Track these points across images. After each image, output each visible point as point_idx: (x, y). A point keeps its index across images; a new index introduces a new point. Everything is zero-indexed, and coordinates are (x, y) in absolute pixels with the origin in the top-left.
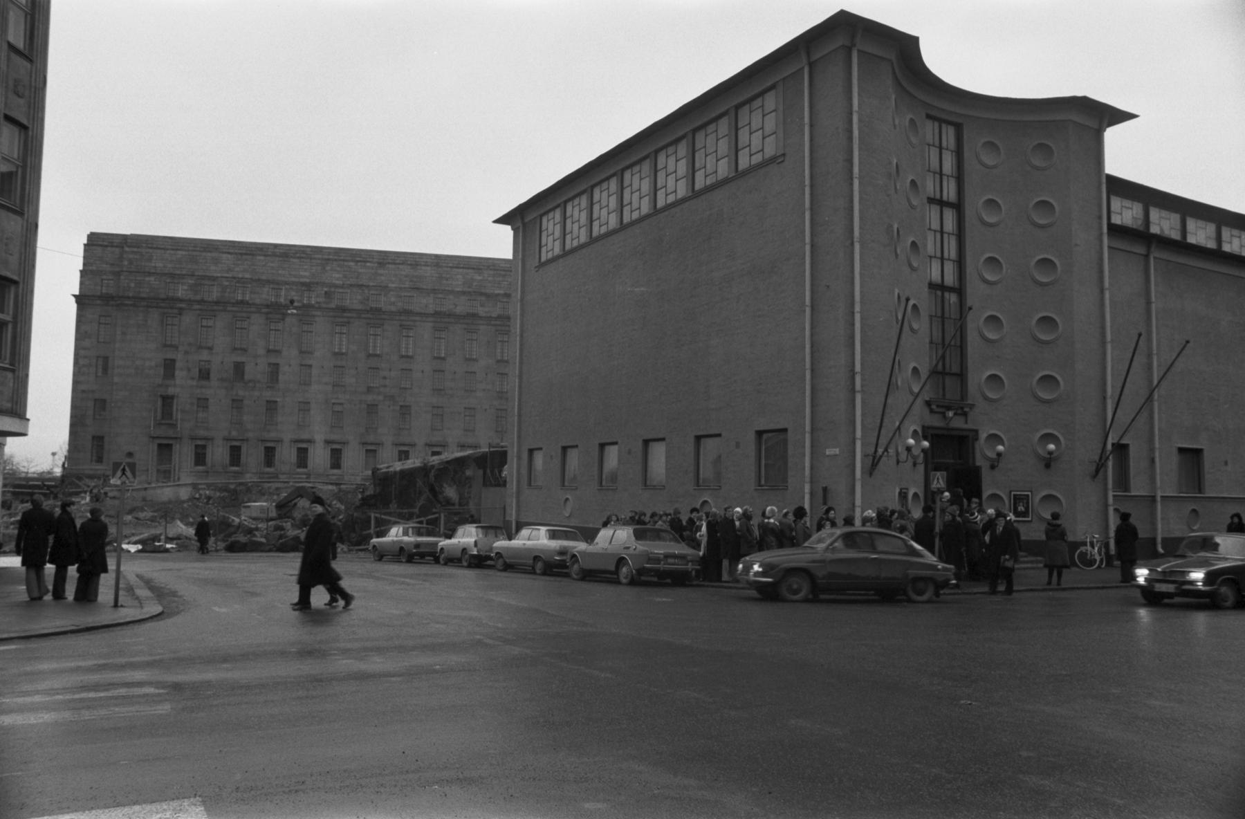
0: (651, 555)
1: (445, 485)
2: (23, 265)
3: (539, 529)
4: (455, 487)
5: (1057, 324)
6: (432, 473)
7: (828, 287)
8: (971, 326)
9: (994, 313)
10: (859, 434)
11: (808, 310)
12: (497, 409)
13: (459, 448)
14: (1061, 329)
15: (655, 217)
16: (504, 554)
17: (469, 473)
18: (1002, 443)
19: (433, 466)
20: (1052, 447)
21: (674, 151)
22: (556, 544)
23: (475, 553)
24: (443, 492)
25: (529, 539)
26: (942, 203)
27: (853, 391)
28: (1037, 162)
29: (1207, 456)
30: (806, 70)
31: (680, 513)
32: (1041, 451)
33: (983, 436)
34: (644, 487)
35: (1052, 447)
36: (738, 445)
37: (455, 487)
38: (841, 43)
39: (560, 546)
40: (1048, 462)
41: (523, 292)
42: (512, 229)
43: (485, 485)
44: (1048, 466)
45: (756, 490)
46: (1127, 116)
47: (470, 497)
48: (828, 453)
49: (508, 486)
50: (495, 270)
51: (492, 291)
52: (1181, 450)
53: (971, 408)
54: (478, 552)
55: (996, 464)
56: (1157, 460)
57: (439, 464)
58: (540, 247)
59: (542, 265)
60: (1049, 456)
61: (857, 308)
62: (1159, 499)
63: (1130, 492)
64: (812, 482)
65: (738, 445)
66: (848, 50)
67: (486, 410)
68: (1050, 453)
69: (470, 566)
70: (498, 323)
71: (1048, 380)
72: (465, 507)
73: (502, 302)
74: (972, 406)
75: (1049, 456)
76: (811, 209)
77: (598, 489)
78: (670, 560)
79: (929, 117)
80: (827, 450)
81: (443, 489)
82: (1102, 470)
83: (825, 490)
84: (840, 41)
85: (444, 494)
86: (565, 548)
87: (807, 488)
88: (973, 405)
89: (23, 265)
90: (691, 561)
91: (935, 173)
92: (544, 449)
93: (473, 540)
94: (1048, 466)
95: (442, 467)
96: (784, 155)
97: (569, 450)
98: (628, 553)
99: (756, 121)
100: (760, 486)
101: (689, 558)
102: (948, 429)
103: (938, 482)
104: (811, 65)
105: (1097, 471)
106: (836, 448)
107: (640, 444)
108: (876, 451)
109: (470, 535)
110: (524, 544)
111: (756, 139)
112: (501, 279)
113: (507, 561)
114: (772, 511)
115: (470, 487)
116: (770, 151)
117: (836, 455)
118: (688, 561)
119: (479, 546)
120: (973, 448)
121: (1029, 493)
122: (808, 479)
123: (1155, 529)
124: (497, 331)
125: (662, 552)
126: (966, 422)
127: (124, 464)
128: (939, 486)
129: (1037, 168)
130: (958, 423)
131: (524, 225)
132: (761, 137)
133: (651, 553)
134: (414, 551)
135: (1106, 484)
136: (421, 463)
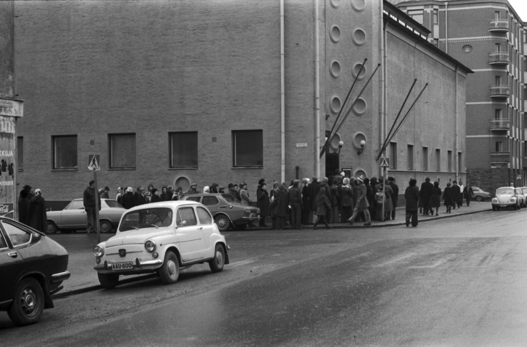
0: (246, 211)
2: (383, 52)
5: (365, 38)
7: (297, 44)
11: (282, 57)
16: (56, 222)
18: (364, 139)
20: (363, 142)
27: (315, 109)
34: (109, 169)
35: (363, 142)
36: (214, 140)
45: (233, 169)
48: (298, 145)
52: (234, 132)
55: (361, 152)
60: (361, 147)
63: (396, 169)
64: (286, 164)
65: (214, 140)
75: (361, 147)
77: (52, 171)
80: (297, 144)
83: (297, 168)
87: (283, 167)
89: (383, 52)
98: (226, 210)
103: (384, 163)
106: (304, 142)
114: (347, 180)
118: (257, 214)
121: (350, 170)
122: (283, 162)
127: (94, 156)
128: (385, 165)
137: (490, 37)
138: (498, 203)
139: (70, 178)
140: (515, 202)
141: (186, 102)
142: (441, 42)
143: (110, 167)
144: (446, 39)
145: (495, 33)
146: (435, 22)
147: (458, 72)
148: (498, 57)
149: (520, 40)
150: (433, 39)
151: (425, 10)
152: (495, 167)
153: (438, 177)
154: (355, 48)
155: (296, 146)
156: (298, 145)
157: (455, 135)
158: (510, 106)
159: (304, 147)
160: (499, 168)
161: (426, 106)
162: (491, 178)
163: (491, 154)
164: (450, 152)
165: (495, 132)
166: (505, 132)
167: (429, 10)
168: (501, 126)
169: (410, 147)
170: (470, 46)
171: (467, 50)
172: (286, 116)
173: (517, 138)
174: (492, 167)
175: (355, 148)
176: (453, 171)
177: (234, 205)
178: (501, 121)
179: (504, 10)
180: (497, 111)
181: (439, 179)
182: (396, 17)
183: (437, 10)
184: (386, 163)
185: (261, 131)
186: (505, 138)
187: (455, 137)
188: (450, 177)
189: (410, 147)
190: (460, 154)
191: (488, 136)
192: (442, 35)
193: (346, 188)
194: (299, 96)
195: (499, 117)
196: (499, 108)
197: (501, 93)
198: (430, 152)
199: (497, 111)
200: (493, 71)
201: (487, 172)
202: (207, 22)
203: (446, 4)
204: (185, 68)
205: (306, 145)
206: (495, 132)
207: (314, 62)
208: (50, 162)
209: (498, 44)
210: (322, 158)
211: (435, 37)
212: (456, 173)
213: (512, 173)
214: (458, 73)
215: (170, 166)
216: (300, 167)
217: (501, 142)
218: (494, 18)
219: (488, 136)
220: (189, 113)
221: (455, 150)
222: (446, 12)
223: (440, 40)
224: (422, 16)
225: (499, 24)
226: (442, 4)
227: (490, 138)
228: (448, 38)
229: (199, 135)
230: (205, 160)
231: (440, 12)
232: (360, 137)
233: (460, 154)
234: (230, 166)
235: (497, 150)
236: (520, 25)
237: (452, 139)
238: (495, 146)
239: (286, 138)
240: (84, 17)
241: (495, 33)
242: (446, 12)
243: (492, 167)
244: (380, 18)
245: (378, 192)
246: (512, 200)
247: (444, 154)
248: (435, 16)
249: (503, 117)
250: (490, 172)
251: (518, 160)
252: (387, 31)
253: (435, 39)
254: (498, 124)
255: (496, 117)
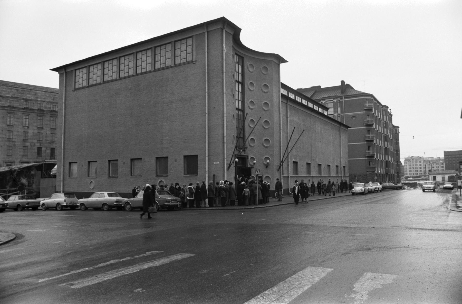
1: (21, 178)
3: (104, 193)
4: (26, 179)
6: (16, 173)
7: (214, 108)
8: (246, 122)
9: (252, 119)
10: (226, 157)
11: (207, 115)
12: (8, 146)
13: (21, 163)
14: (270, 125)
15: (137, 77)
16: (85, 204)
17: (33, 173)
19: (15, 170)
20: (268, 161)
21: (146, 53)
22: (114, 199)
23: (65, 204)
24: (21, 181)
25: (99, 197)
26: (239, 82)
27: (224, 143)
28: (264, 72)
29: (299, 163)
30: (206, 33)
31: (303, 181)
32: (265, 163)
33: (250, 157)
35: (268, 161)
36: (176, 161)
37: (26, 179)
38: (220, 27)
39: (116, 199)
40: (267, 166)
41: (65, 100)
42: (59, 73)
43: (42, 177)
44: (267, 167)
46: (286, 61)
47: (33, 183)
48: (214, 163)
49: (57, 178)
50: (7, 86)
51: (5, 95)
52: (185, 157)
53: (246, 149)
54: (66, 204)
56: (289, 165)
57: (19, 169)
58: (75, 82)
59: (76, 89)
60: (267, 164)
61: (225, 115)
62: (290, 177)
64: (208, 173)
65: (176, 161)
66: (222, 30)
67: (2, 146)
68: (268, 163)
69: (62, 210)
70: (8, 109)
71: (267, 140)
72: (31, 187)
73: (10, 100)
74: (247, 148)
75: (267, 164)
76: (208, 81)
78: (172, 202)
79: (236, 54)
81: (21, 180)
82: (280, 169)
83: (214, 175)
84: (220, 26)
85: (21, 182)
86: (118, 200)
87: (207, 175)
88: (247, 148)
90: (179, 201)
91: (237, 72)
92: (78, 163)
93: (64, 199)
94: (267, 167)
95: (20, 170)
96: (196, 61)
97: (72, 164)
99: (184, 47)
100: (185, 175)
101: (178, 200)
102: (240, 155)
103: (258, 172)
104: (208, 32)
105: (279, 169)
107: (129, 160)
108: (231, 162)
109: (61, 197)
110: (55, 200)
111: (184, 54)
112: (9, 90)
113: (87, 206)
114: (222, 182)
115: (33, 178)
116: (189, 59)
117: (218, 164)
118: (178, 202)
119: (66, 201)
120: (247, 161)
122: (207, 172)
123: (289, 186)
124: (8, 112)
125: (170, 199)
126: (245, 153)
128: (258, 173)
129: (263, 74)
130: (243, 154)
131: (66, 73)
132: (186, 54)
133: (167, 199)
134: (27, 206)
135: (281, 173)
136: (8, 169)
137: (364, 112)
138: (354, 191)
139: (115, 181)
140: (363, 191)
141: (163, 141)
142: (341, 115)
143: (132, 175)
144: (344, 114)
145: (366, 110)
146: (339, 106)
147: (341, 127)
148: (368, 121)
149: (381, 113)
150: (337, 114)
151: (334, 100)
152: (369, 173)
153: (320, 179)
154: (264, 112)
155: (213, 164)
156: (214, 163)
157: (341, 158)
158: (379, 146)
159: (218, 164)
160: (370, 174)
161: (320, 144)
162: (367, 178)
163: (367, 167)
164: (337, 166)
165: (368, 157)
166: (373, 157)
167: (335, 101)
168: (371, 153)
169: (308, 164)
170: (355, 117)
171: (354, 119)
172: (208, 147)
173: (381, 159)
174: (367, 173)
175: (265, 165)
176: (340, 175)
177: (161, 197)
178: (371, 151)
179: (371, 99)
180: (369, 147)
181: (330, 179)
182: (301, 98)
183: (339, 100)
184: (259, 172)
185: (197, 155)
186: (374, 159)
187: (341, 159)
188: (337, 178)
189: (308, 164)
190: (344, 167)
191: (365, 158)
192: (342, 112)
193: (222, 186)
194: (215, 136)
195: (370, 149)
196: (370, 145)
197: (371, 138)
198: (323, 167)
199: (369, 147)
200: (366, 128)
201: (365, 175)
202: (173, 99)
203: (343, 97)
204: (163, 124)
205: (218, 163)
206: (368, 157)
207: (223, 117)
208: (107, 173)
209: (368, 115)
210: (230, 170)
211: (339, 113)
212: (341, 176)
213: (392, 176)
214: (342, 128)
215: (157, 175)
216: (215, 175)
217: (371, 161)
218: (366, 103)
219: (365, 158)
220: (164, 147)
221: (341, 165)
222: (344, 101)
223: (341, 114)
224: (332, 103)
225: (368, 106)
226: (341, 97)
227: (365, 159)
228: (345, 113)
229: (169, 159)
230: (172, 171)
231: (341, 101)
232: (267, 158)
233: (344, 167)
234: (183, 175)
235: (370, 165)
236: (381, 107)
237: (339, 161)
238: (368, 163)
239: (208, 159)
240: (122, 100)
241: (366, 110)
242: (344, 101)
243: (367, 173)
244: (279, 96)
245: (245, 189)
246: (362, 190)
247: (333, 168)
248: (338, 103)
249: (372, 149)
250: (367, 175)
251: (382, 169)
252: (289, 105)
253: (339, 114)
254: (369, 153)
255: (369, 149)
